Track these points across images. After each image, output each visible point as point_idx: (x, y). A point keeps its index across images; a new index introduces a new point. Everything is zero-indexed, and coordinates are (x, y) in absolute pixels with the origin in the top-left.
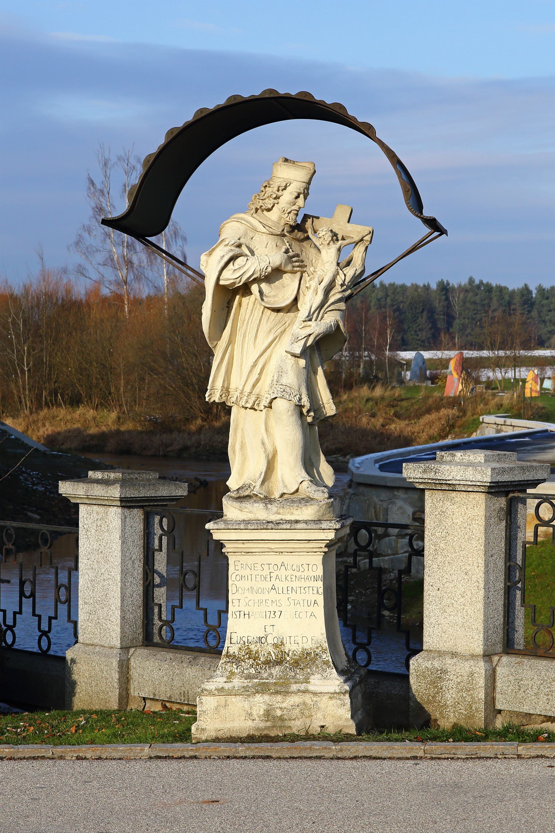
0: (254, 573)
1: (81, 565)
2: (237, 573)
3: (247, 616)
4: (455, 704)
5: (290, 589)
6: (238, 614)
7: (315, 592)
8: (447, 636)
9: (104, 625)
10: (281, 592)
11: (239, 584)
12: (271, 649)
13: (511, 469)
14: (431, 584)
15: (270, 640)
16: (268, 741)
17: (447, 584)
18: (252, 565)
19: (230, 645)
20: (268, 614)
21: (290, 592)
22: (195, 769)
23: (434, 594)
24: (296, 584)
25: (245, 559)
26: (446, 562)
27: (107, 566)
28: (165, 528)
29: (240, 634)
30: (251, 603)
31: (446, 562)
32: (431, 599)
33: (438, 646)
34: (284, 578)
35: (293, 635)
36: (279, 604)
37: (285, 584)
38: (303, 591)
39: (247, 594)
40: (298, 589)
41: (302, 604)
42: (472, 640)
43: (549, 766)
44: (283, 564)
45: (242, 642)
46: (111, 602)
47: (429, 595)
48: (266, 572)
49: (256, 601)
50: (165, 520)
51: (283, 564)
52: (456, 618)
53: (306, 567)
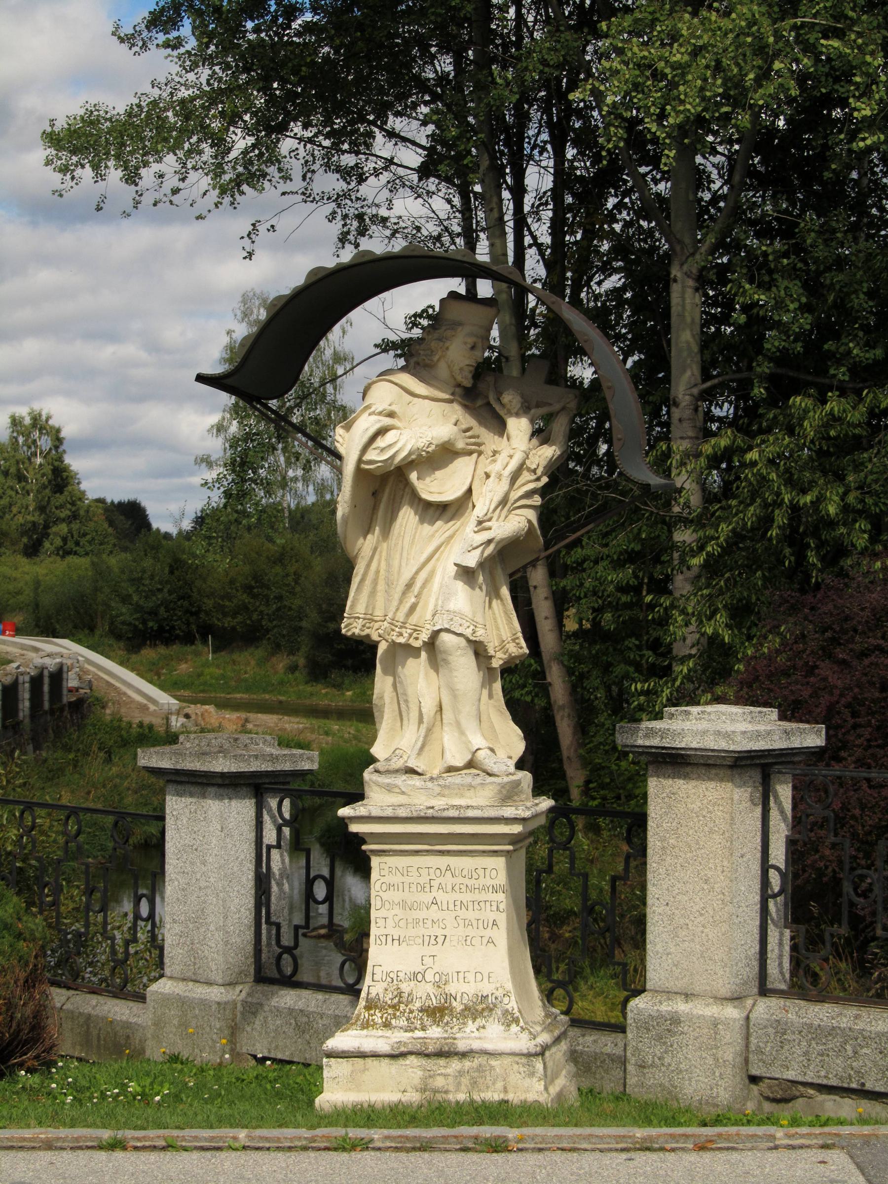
0: (407, 880)
1: (168, 868)
2: (383, 880)
3: (396, 942)
5: (458, 903)
6: (383, 939)
7: (494, 908)
10: (445, 907)
11: (385, 896)
12: (430, 989)
13: (769, 733)
15: (429, 976)
16: (426, 1123)
17: (679, 897)
19: (372, 983)
20: (427, 939)
21: (458, 908)
22: (310, 1168)
23: (660, 910)
24: (467, 897)
25: (392, 861)
27: (204, 869)
28: (287, 816)
29: (386, 968)
30: (402, 923)
32: (656, 918)
34: (449, 888)
35: (463, 969)
36: (442, 925)
37: (452, 897)
38: (476, 906)
39: (396, 910)
40: (470, 904)
41: (475, 925)
42: (715, 977)
43: (820, 1162)
44: (448, 868)
45: (389, 980)
48: (424, 879)
49: (410, 920)
50: (287, 803)
51: (448, 868)
52: (692, 945)
53: (481, 872)
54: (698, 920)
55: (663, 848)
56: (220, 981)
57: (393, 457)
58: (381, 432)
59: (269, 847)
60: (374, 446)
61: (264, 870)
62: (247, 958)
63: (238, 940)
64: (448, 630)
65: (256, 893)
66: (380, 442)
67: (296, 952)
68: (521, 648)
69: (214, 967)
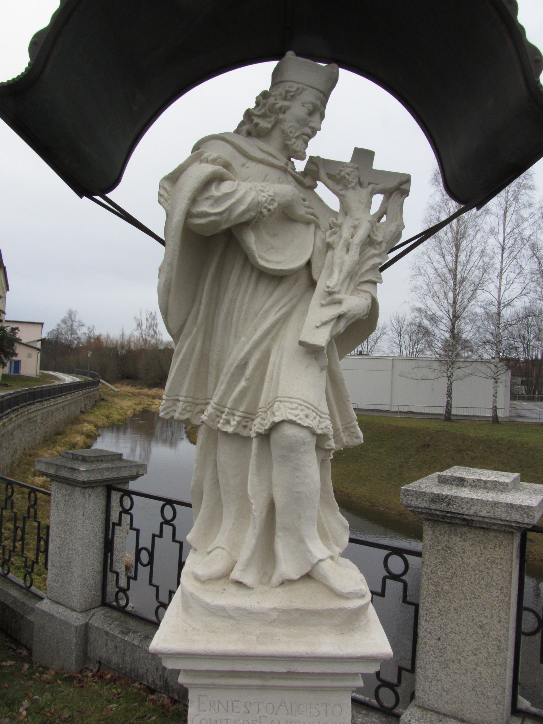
8: (449, 697)
17: (452, 636)
18: (230, 703)
23: (432, 643)
26: (452, 608)
31: (452, 608)
32: (427, 648)
33: (436, 706)
54: (471, 658)
56: (79, 610)
57: (230, 210)
58: (215, 179)
59: (114, 524)
60: (207, 195)
61: (110, 536)
62: (97, 592)
64: (292, 422)
66: (215, 191)
68: (358, 437)
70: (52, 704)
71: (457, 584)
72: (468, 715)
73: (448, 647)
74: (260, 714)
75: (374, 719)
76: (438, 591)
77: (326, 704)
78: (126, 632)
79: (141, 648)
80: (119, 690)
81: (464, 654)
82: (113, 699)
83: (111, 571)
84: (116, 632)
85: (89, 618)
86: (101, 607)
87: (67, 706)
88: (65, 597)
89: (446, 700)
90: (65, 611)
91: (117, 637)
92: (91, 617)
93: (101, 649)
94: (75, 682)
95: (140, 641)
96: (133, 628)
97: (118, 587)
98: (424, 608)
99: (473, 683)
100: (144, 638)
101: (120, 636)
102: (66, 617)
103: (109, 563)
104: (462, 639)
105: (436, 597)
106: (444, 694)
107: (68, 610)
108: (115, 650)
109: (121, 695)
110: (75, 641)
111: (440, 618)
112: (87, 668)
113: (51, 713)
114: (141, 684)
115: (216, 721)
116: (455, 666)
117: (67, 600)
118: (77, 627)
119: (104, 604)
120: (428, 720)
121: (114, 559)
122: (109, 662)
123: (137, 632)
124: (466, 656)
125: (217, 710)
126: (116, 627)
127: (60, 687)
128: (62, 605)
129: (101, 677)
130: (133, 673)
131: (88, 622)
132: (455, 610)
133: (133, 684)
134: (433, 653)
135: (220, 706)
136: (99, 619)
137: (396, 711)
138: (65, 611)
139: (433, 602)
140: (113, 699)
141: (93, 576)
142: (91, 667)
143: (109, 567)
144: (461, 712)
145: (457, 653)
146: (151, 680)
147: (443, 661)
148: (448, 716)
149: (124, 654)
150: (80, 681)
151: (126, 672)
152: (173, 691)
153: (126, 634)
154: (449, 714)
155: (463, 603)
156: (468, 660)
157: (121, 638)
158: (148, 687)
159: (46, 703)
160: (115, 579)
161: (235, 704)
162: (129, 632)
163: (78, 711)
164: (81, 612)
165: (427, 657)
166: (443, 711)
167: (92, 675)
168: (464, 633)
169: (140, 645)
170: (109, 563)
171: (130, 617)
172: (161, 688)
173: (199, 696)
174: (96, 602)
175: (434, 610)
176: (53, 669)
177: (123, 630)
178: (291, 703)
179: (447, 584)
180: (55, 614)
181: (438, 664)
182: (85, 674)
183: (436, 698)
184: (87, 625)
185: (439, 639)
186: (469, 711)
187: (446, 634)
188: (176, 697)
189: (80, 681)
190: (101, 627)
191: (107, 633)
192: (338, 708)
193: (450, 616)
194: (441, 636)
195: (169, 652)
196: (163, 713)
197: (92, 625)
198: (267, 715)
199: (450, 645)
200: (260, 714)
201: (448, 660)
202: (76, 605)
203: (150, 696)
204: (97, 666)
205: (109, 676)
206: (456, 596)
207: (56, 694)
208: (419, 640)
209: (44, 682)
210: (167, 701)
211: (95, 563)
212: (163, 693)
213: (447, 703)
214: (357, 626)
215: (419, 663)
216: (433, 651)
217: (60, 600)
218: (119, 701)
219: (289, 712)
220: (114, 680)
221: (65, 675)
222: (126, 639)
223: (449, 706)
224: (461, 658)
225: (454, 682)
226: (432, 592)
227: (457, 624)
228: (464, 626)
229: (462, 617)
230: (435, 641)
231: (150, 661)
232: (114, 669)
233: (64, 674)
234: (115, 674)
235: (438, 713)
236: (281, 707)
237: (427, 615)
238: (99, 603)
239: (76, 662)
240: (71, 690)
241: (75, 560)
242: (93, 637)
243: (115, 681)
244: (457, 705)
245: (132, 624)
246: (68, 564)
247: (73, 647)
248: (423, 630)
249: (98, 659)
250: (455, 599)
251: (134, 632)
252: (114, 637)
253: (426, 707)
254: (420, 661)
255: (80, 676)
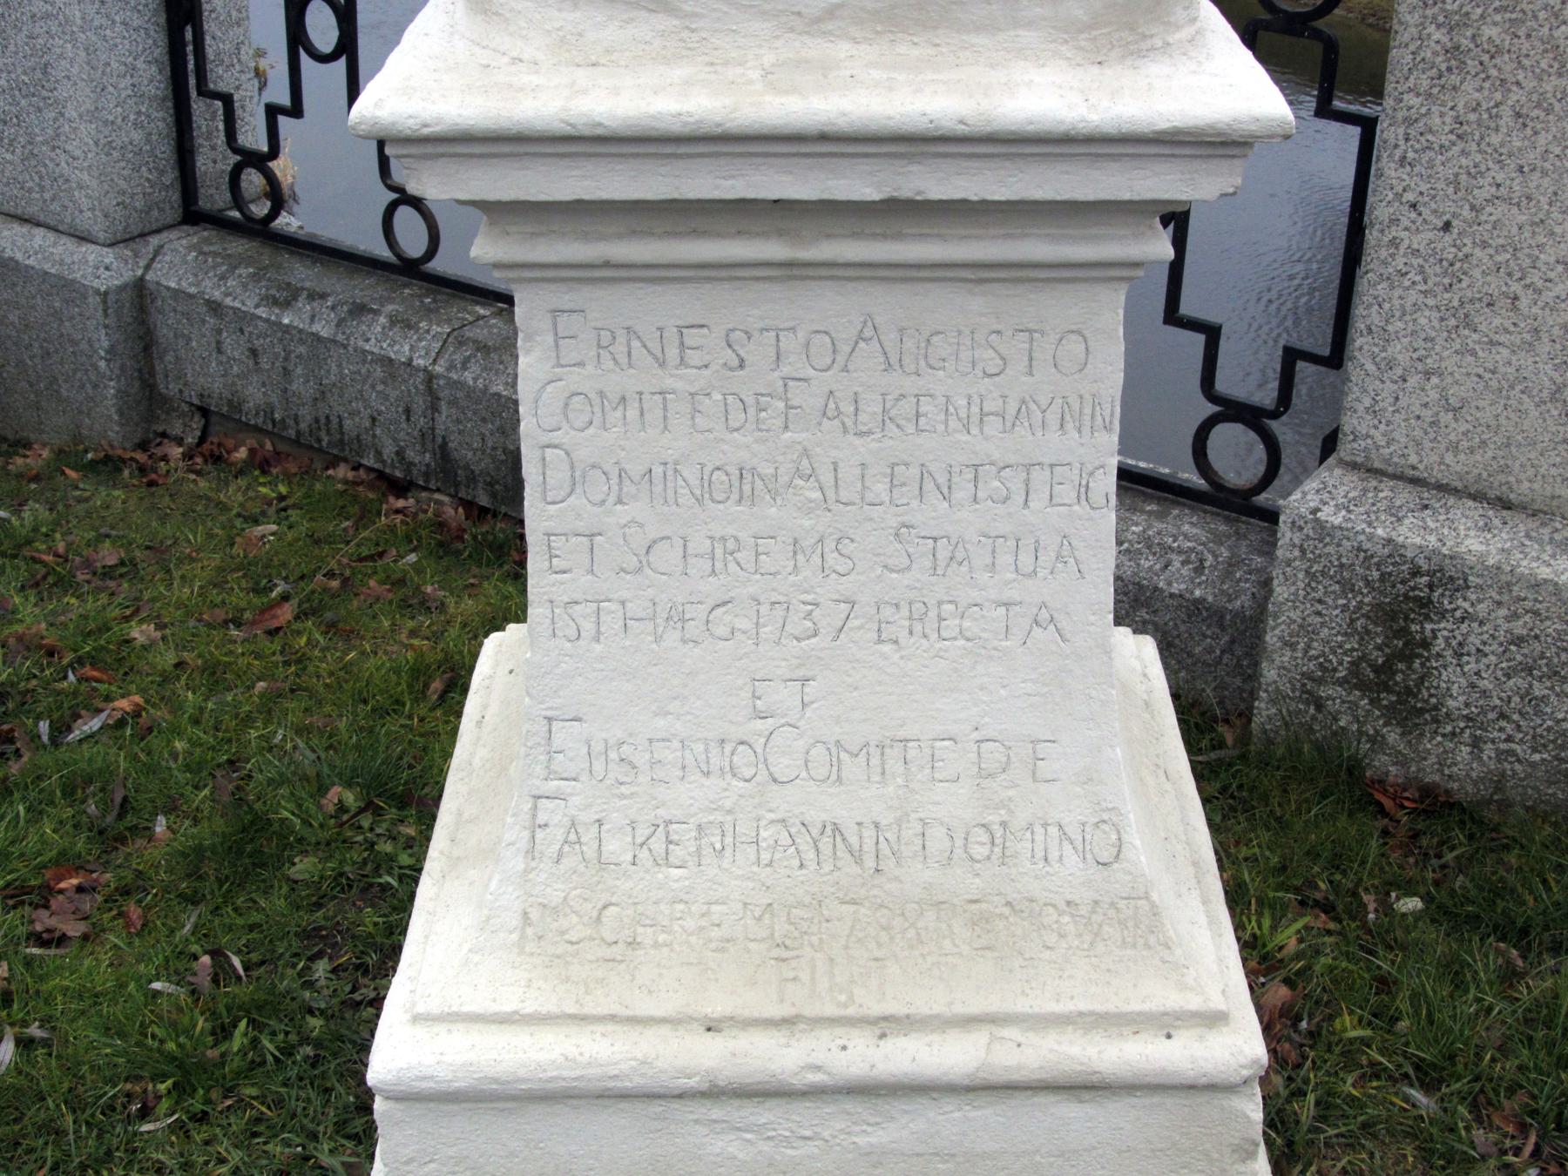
4: (1483, 712)
8: (1463, 427)
9: (51, 165)
14: (1410, 197)
17: (1499, 211)
18: (671, 334)
23: (1419, 241)
26: (1506, 112)
30: (667, 556)
31: (1506, 112)
32: (1399, 263)
33: (1413, 459)
46: (63, 92)
47: (1395, 243)
49: (699, 544)
52: (1525, 360)
55: (1454, 51)
62: (162, 172)
63: (137, 136)
65: (169, 21)
67: (275, 166)
69: (85, 203)
70: (53, 531)
71: (1535, 17)
72: (1527, 484)
73: (1478, 252)
74: (786, 370)
75: (1186, 527)
76: (1457, 48)
77: (1030, 331)
78: (287, 297)
79: (345, 347)
80: (283, 489)
81: (1535, 278)
82: (263, 513)
83: (203, 92)
84: (247, 301)
85: (142, 263)
86: (185, 227)
87: (108, 536)
88: (47, 196)
89: (1453, 437)
90: (55, 244)
91: (255, 317)
92: (153, 260)
93: (203, 367)
94: (126, 472)
95: (338, 325)
96: (307, 284)
97: (236, 150)
98: (1400, 115)
99: (1556, 375)
100: (350, 312)
101: (262, 312)
102: (62, 262)
103: (191, 66)
104: (1533, 224)
105: (1449, 69)
106: (1446, 418)
107: (64, 239)
108: (251, 363)
109: (290, 502)
110: (106, 344)
111: (1456, 150)
112: (164, 435)
113: (57, 555)
114: (355, 468)
115: (623, 399)
116: (1497, 321)
117: (55, 207)
118: (106, 293)
119: (192, 215)
120: (1382, 506)
121: (210, 52)
122: (236, 405)
123: (323, 296)
124: (1540, 284)
125: (623, 360)
126: (245, 286)
127: (77, 488)
128: (38, 225)
129: (216, 459)
130: (323, 434)
131: (142, 279)
132: (1518, 115)
133: (330, 472)
134: (1418, 278)
135: (636, 344)
136: (181, 264)
137: (1262, 499)
138: (55, 244)
139: (1435, 91)
140: (263, 513)
141: (139, 113)
142: (176, 429)
143: (192, 81)
144: (1502, 478)
145: (1510, 275)
146: (389, 451)
147: (1456, 303)
148: (1455, 492)
149: (286, 372)
150: (142, 470)
151: (298, 433)
152: (472, 479)
153: (286, 304)
154: (1459, 485)
155: (1549, 88)
156: (1548, 296)
157: (267, 321)
158: (381, 475)
159: (35, 530)
160: (221, 126)
161: (692, 337)
162: (295, 299)
163: (148, 548)
164: (111, 245)
165: (1397, 292)
166: (1438, 475)
167: (183, 454)
168: (1544, 200)
169: (340, 337)
170: (191, 66)
171: (292, 253)
172: (427, 475)
173: (556, 312)
174: (161, 210)
175: (1438, 121)
176: (44, 445)
177: (273, 292)
178: (902, 330)
179: (1498, 18)
180: (19, 256)
181: (1435, 314)
182: (159, 451)
183: (1418, 433)
184: (139, 285)
185: (1447, 226)
186: (1531, 472)
187: (1473, 208)
188: (484, 500)
189: (142, 470)
190: (193, 290)
191: (215, 307)
192: (1074, 346)
193: (1495, 139)
194: (1454, 215)
195: (426, 131)
196: (441, 544)
197: (158, 283)
198: (811, 372)
199: (1484, 245)
200: (786, 370)
201: (1471, 301)
202: (88, 220)
203: (391, 499)
204: (197, 423)
205: (242, 453)
206: (1526, 62)
207: (68, 506)
208: (1371, 236)
209: (20, 476)
210: (453, 514)
211: (140, 64)
212: (438, 490)
213: (1454, 448)
214: (1159, 43)
215: (1360, 342)
216: (1422, 271)
217: (33, 210)
218: (287, 518)
219: (894, 360)
220: (261, 464)
221: (90, 456)
222: (286, 321)
223: (1462, 457)
224: (1520, 292)
225: (1487, 376)
226: (1436, 54)
227: (1521, 169)
228: (1545, 173)
229: (1542, 140)
230: (1430, 235)
231: (380, 387)
232: (257, 429)
233: (86, 451)
234: (262, 446)
235: (1415, 481)
236: (862, 344)
237: (1407, 140)
238: (173, 212)
239: (121, 413)
240: (116, 493)
241: (61, 56)
242: (166, 326)
243: (264, 466)
244: (1490, 454)
245: (302, 273)
246: (38, 74)
247: (102, 364)
248: (1391, 196)
249: (196, 401)
250: (1520, 77)
251: (312, 296)
252: (243, 318)
253: (1377, 465)
254: (1370, 306)
255: (141, 457)
